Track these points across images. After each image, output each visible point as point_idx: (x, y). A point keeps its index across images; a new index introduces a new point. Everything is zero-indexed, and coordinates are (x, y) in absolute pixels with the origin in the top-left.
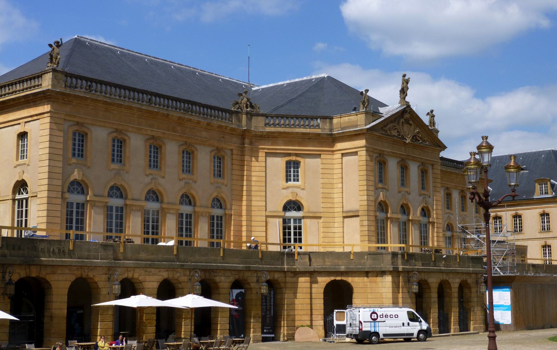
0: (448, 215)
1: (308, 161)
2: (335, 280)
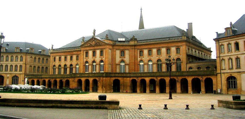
0: (158, 57)
1: (182, 47)
2: (195, 78)
